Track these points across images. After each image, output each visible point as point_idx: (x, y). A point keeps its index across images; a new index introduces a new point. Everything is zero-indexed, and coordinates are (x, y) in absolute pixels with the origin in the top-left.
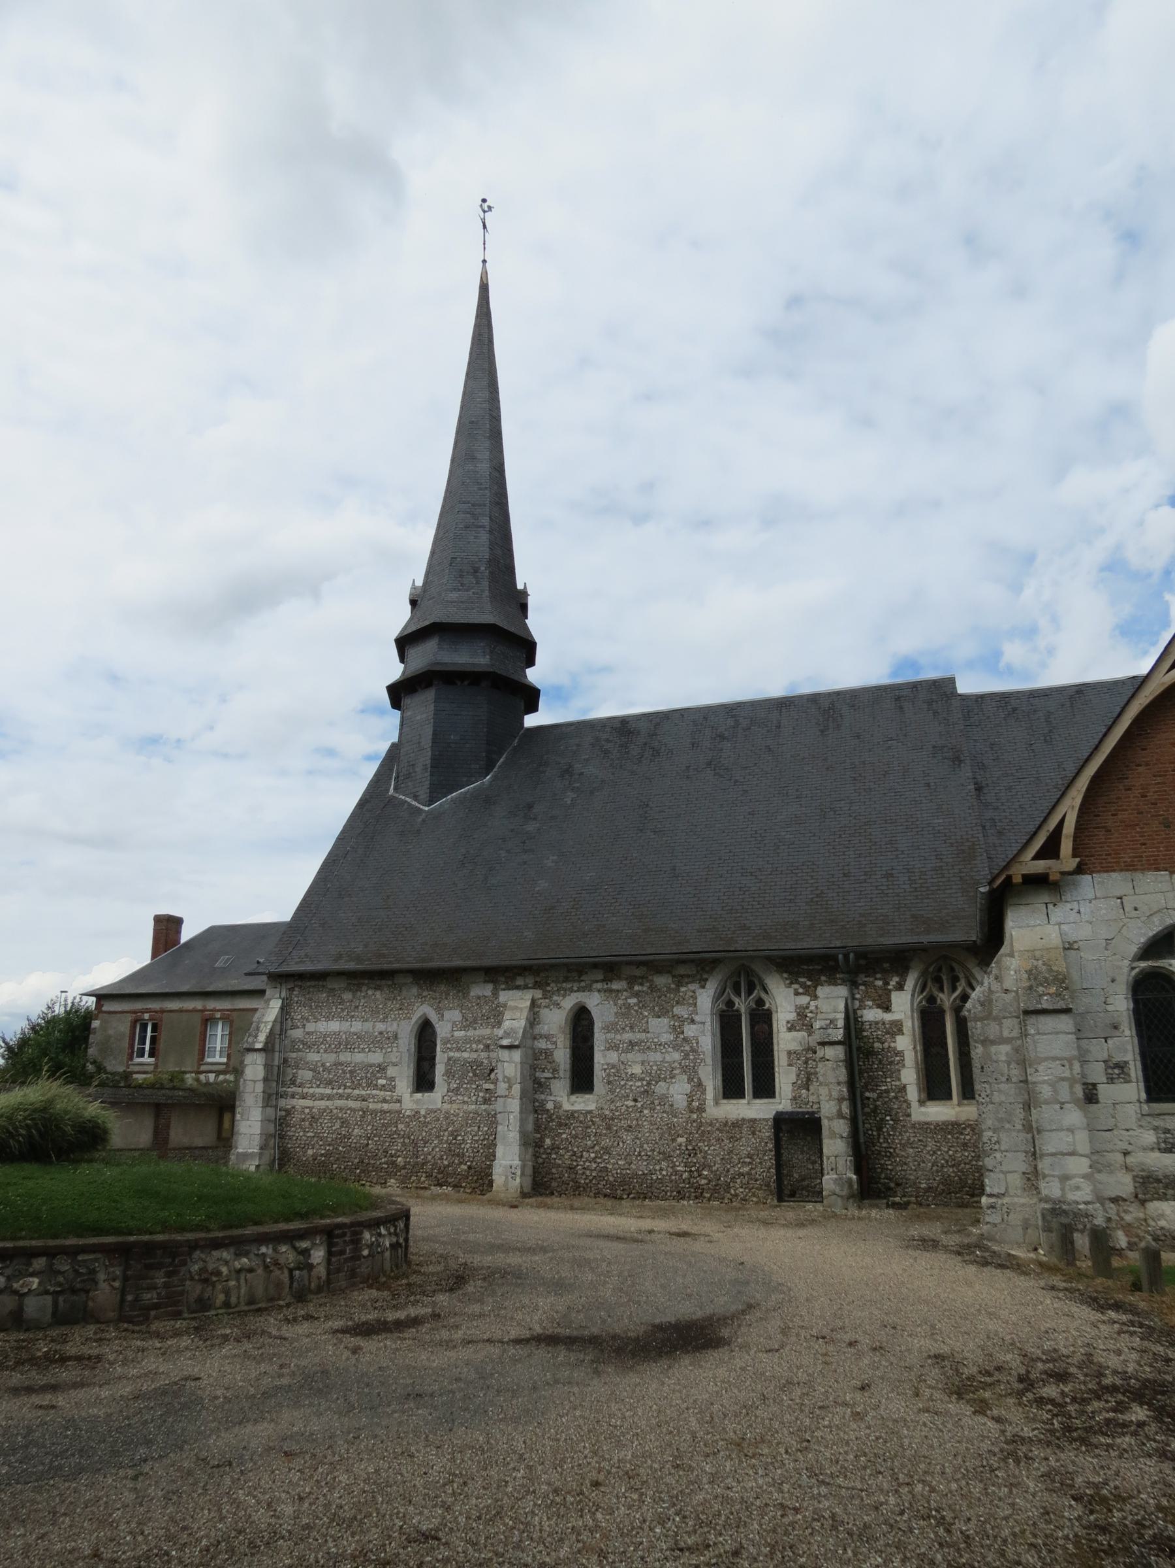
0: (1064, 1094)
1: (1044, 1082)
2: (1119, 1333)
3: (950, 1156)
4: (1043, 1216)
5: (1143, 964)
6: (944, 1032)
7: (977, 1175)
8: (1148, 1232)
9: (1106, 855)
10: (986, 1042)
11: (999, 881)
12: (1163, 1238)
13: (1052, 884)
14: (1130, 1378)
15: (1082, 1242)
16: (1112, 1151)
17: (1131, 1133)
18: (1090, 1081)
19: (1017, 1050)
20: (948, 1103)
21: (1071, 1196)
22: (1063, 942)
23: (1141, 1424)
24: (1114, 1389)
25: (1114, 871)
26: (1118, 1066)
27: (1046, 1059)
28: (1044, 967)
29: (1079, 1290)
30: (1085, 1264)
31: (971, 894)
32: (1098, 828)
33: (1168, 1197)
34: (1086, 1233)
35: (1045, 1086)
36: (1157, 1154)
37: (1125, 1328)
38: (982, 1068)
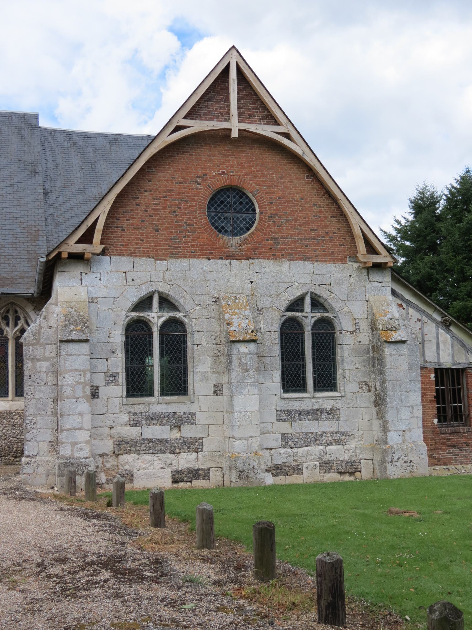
0: (79, 393)
1: (68, 385)
2: (97, 532)
3: (4, 433)
4: (59, 467)
5: (134, 314)
6: (7, 353)
7: (20, 444)
8: (118, 473)
9: (121, 245)
10: (35, 359)
11: (53, 255)
12: (126, 476)
13: (86, 260)
14: (102, 556)
15: (81, 481)
16: (104, 426)
17: (115, 415)
18: (95, 385)
19: (53, 365)
20: (5, 399)
21: (77, 455)
22: (88, 298)
23: (106, 581)
24: (93, 563)
25: (124, 255)
26: (112, 375)
27: (70, 371)
28: (75, 313)
29: (76, 509)
30: (81, 494)
31: (34, 263)
32: (117, 227)
33: (132, 452)
34: (84, 475)
35: (68, 388)
36: (128, 427)
37: (101, 528)
38: (30, 376)
